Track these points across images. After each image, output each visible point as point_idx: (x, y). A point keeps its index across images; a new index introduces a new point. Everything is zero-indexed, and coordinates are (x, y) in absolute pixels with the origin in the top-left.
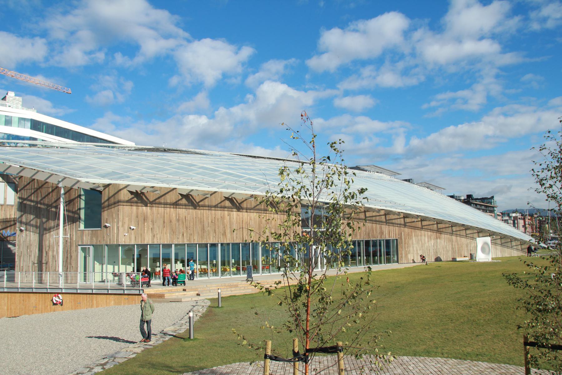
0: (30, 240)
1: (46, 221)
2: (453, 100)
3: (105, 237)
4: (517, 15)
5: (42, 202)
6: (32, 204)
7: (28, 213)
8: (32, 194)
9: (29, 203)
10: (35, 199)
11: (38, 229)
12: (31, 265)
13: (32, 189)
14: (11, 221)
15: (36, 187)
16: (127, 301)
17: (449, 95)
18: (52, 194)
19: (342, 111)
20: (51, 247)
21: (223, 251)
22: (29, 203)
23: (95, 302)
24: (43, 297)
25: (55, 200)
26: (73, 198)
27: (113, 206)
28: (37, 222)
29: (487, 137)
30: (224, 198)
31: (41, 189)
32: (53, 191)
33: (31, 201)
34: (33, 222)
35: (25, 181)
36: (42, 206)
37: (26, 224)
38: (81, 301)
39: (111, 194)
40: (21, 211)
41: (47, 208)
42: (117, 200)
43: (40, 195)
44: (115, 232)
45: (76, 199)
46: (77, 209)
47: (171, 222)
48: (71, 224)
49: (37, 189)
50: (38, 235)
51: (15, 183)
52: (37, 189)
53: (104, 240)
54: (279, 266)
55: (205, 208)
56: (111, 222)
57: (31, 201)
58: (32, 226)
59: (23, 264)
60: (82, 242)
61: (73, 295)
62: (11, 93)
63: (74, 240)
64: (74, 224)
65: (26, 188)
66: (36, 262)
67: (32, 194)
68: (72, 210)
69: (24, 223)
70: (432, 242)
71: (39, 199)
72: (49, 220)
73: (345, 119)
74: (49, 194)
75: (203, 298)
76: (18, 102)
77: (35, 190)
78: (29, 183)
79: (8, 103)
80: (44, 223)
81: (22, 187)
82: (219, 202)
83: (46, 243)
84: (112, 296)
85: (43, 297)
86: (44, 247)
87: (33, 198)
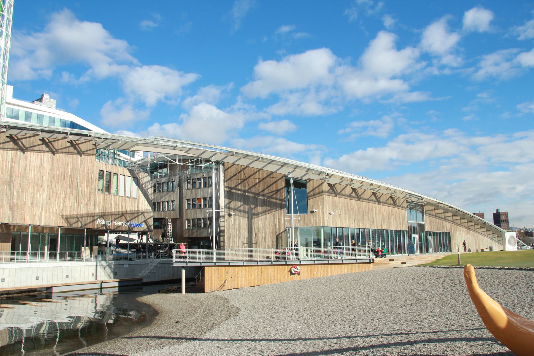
0: (239, 224)
1: (254, 208)
2: (365, 128)
3: (312, 221)
4: (425, 61)
5: (250, 191)
6: (240, 192)
7: (235, 201)
8: (239, 184)
9: (236, 191)
10: (242, 188)
11: (247, 214)
12: (240, 245)
13: (238, 180)
14: (135, 213)
15: (242, 178)
16: (358, 269)
17: (362, 124)
18: (259, 185)
19: (267, 133)
20: (260, 229)
21: (391, 233)
22: (236, 191)
24: (281, 268)
25: (263, 189)
26: (280, 188)
27: (318, 195)
28: (245, 208)
29: (391, 160)
30: (372, 193)
31: (248, 180)
32: (259, 182)
33: (239, 190)
34: (242, 208)
35: (231, 173)
36: (250, 195)
37: (234, 210)
38: (317, 270)
40: (229, 199)
41: (255, 196)
42: (321, 190)
43: (247, 185)
44: (321, 216)
45: (283, 189)
46: (284, 197)
48: (279, 210)
49: (244, 180)
50: (247, 219)
51: (137, 178)
52: (244, 180)
53: (311, 223)
56: (317, 208)
57: (239, 190)
58: (241, 211)
59: (233, 244)
61: (309, 266)
62: (46, 95)
63: (283, 223)
64: (282, 210)
65: (232, 179)
66: (246, 243)
67: (239, 184)
68: (280, 198)
69: (232, 209)
70: (466, 236)
71: (247, 189)
72: (257, 206)
73: (268, 140)
74: (256, 184)
75: (408, 265)
76: (52, 104)
77: (242, 180)
78: (236, 175)
79: (44, 104)
80: (252, 209)
81: (229, 178)
82: (370, 196)
83: (255, 226)
84: (345, 265)
85: (281, 268)
86: (253, 229)
87: (240, 187)
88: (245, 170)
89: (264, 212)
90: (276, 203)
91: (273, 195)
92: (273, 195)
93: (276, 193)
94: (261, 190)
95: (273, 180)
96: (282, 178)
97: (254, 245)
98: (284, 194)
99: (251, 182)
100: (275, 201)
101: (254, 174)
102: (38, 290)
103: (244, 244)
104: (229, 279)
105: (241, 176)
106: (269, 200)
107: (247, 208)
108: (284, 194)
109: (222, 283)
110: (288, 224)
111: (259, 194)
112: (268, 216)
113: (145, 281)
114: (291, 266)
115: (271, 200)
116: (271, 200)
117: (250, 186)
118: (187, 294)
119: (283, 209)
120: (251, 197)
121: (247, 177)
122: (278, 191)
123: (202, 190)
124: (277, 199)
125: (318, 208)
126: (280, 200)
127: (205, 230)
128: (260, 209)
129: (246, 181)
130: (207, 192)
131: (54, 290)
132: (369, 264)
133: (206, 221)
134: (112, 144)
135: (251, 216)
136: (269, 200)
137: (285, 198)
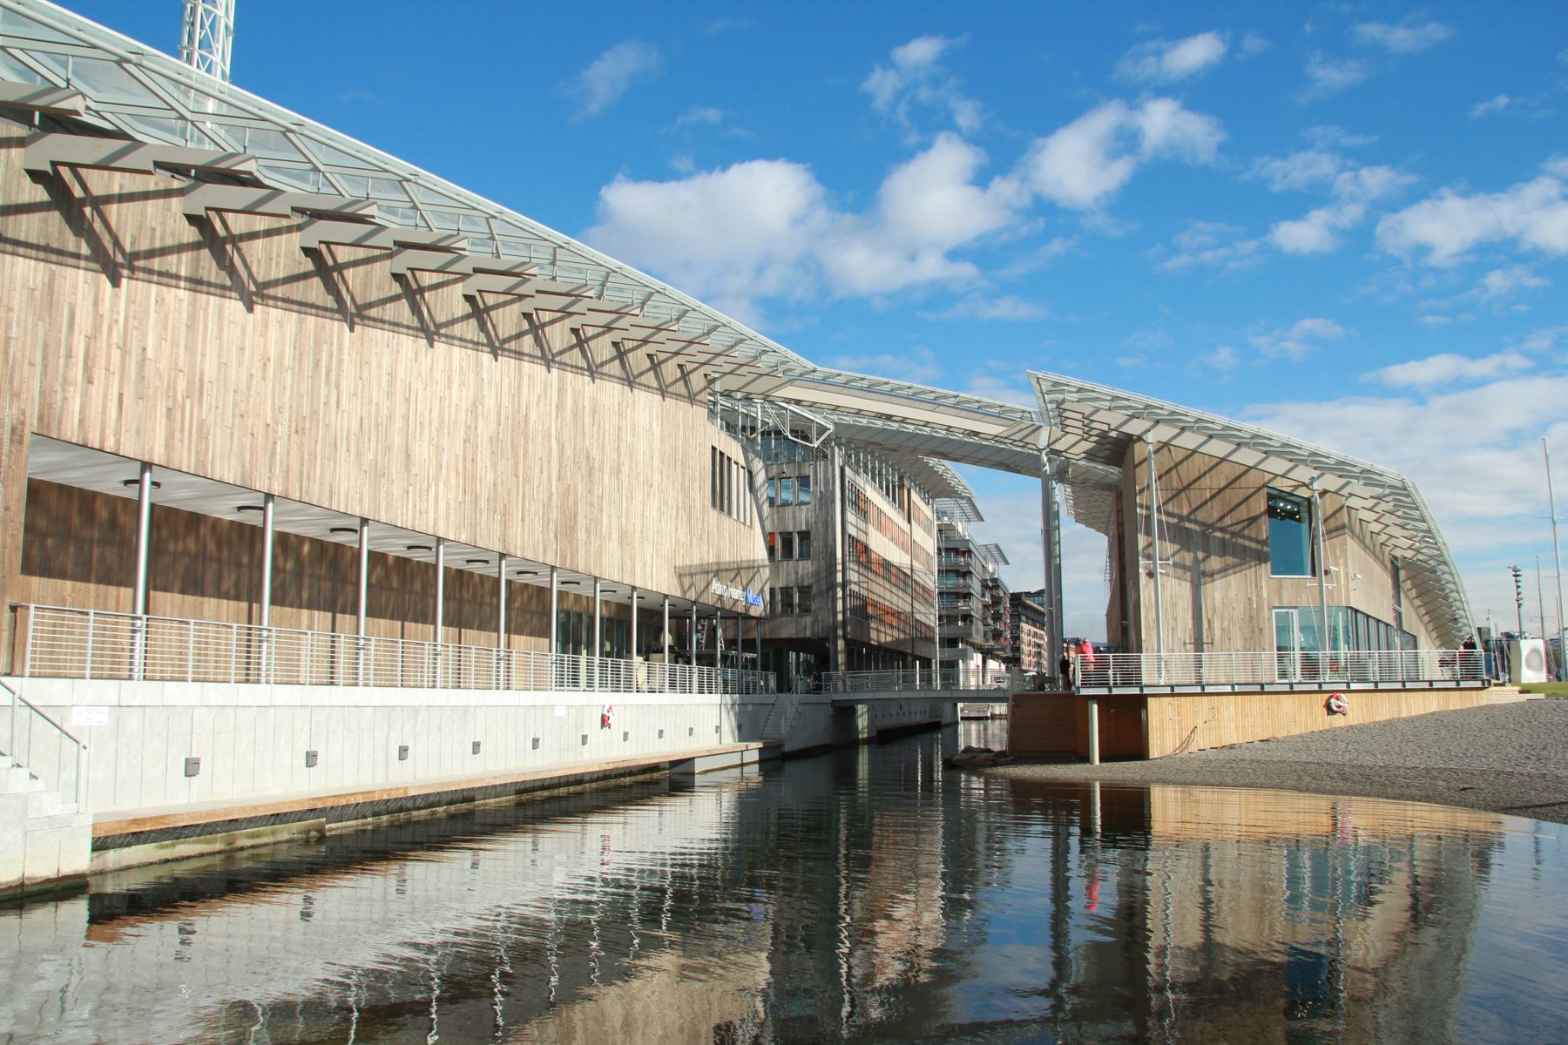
1: (1204, 559)
5: (1192, 517)
23: (1404, 706)
28: (1184, 559)
32: (1212, 497)
39: (1329, 512)
46: (1265, 537)
47: (138, 432)
49: (1180, 492)
50: (1188, 584)
52: (1180, 492)
54: (552, 999)
55: (401, 330)
60: (1280, 600)
74: (1206, 502)
83: (1206, 604)
88: (1180, 468)
89: (1224, 570)
90: (1250, 548)
91: (1243, 529)
92: (1243, 529)
93: (1249, 525)
94: (1216, 516)
95: (1242, 494)
96: (1259, 489)
97: (1205, 646)
98: (1264, 528)
99: (1196, 497)
100: (1247, 543)
101: (1199, 478)
102: (662, 766)
103: (1185, 644)
104: (1200, 725)
105: (1171, 482)
106: (1234, 540)
107: (1188, 558)
108: (1264, 528)
109: (1185, 735)
110: (1277, 600)
111: (1211, 526)
112: (1234, 579)
113: (788, 748)
114: (1328, 695)
115: (1240, 541)
116: (1240, 541)
117: (1194, 506)
118: (1104, 764)
119: (1265, 562)
120: (1196, 531)
121: (1185, 484)
122: (1253, 520)
123: (778, 512)
124: (1250, 539)
125: (1337, 565)
126: (1258, 541)
127: (789, 619)
128: (1215, 562)
129: (1183, 494)
130: (794, 518)
131: (699, 766)
132: (1480, 692)
133: (791, 596)
134: (721, 377)
135: (1199, 578)
136: (1234, 540)
137: (1267, 538)
